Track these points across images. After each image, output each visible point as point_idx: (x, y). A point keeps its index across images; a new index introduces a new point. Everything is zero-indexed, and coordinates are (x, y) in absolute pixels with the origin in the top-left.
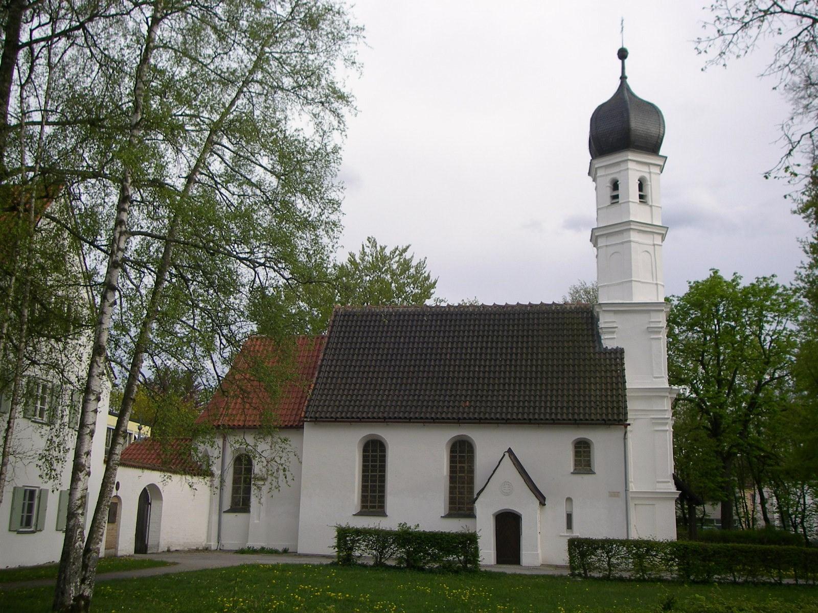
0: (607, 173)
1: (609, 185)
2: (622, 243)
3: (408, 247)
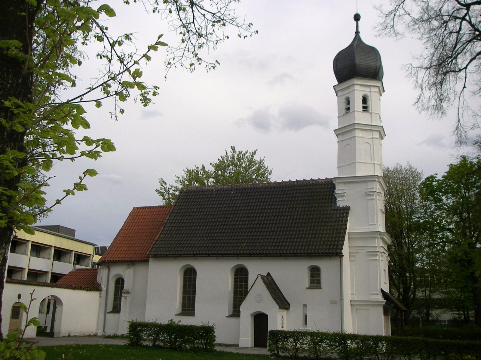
0: (343, 94)
1: (344, 101)
2: (351, 138)
3: (255, 152)
